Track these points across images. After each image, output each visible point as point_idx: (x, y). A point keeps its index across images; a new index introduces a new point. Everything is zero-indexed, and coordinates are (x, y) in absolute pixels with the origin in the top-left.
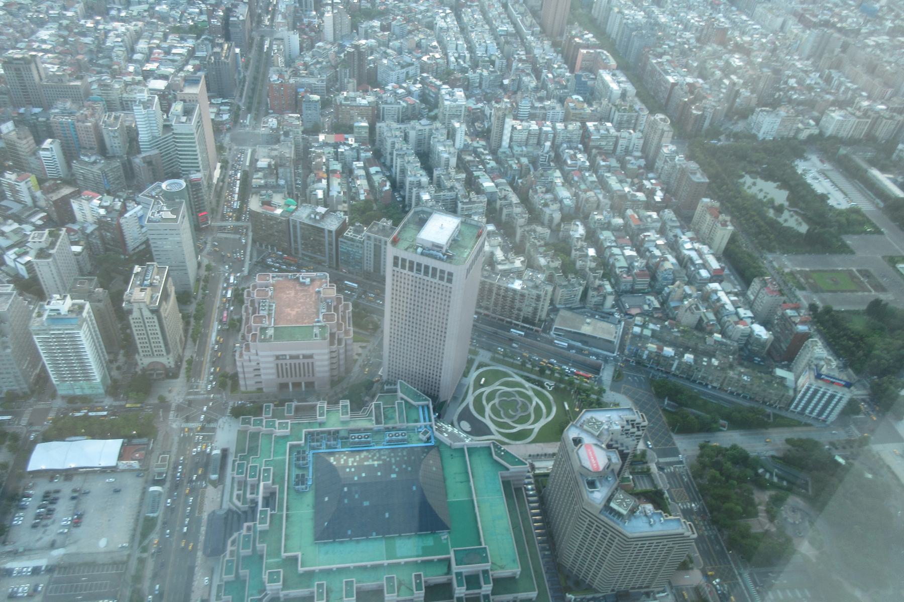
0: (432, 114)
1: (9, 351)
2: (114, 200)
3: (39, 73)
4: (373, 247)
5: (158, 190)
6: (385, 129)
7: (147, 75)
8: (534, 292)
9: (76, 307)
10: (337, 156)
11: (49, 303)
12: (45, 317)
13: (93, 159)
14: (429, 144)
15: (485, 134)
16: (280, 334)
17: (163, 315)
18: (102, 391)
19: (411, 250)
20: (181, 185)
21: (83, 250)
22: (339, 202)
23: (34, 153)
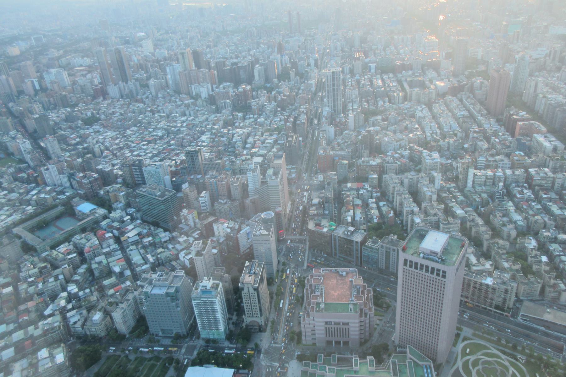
0: (417, 168)
1: (179, 309)
4: (385, 252)
7: (253, 155)
11: (202, 282)
13: (225, 201)
15: (455, 179)
17: (260, 292)
18: (224, 337)
19: (416, 255)
22: (361, 224)
23: (197, 199)
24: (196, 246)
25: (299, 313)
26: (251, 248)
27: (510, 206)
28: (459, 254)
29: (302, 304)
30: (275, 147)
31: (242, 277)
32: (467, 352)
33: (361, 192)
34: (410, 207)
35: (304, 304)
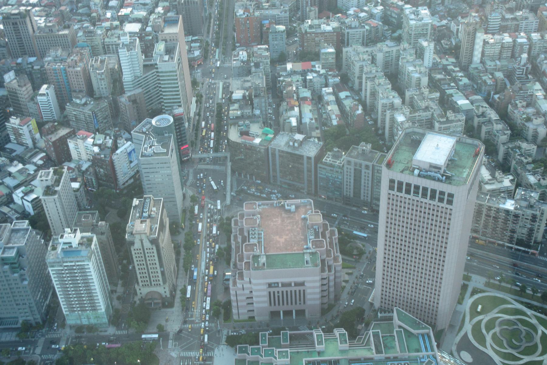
0: (396, 35)
1: (26, 283)
2: (105, 138)
3: (32, 25)
4: (353, 171)
5: (149, 126)
6: (353, 53)
7: (123, 20)
8: (529, 212)
9: (85, 240)
10: (305, 83)
11: (62, 237)
12: (59, 250)
13: (84, 101)
14: (398, 64)
15: (455, 51)
16: (272, 262)
17: (161, 245)
18: (105, 320)
19: (408, 172)
20: (169, 121)
21: (81, 186)
22: (312, 129)
23: (32, 99)
24: (43, 178)
25: (224, 275)
26: (137, 177)
27: (537, 90)
28: (472, 167)
29: (228, 262)
30: (160, 4)
31: (129, 224)
32: (479, 310)
33: (309, 77)
34: (387, 97)
35: (233, 260)
